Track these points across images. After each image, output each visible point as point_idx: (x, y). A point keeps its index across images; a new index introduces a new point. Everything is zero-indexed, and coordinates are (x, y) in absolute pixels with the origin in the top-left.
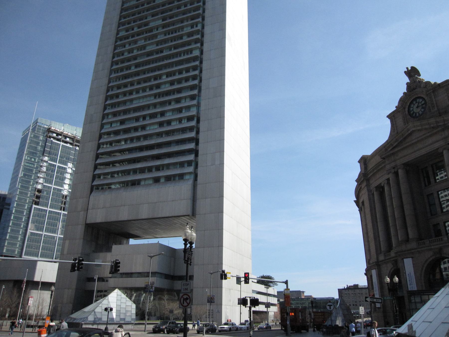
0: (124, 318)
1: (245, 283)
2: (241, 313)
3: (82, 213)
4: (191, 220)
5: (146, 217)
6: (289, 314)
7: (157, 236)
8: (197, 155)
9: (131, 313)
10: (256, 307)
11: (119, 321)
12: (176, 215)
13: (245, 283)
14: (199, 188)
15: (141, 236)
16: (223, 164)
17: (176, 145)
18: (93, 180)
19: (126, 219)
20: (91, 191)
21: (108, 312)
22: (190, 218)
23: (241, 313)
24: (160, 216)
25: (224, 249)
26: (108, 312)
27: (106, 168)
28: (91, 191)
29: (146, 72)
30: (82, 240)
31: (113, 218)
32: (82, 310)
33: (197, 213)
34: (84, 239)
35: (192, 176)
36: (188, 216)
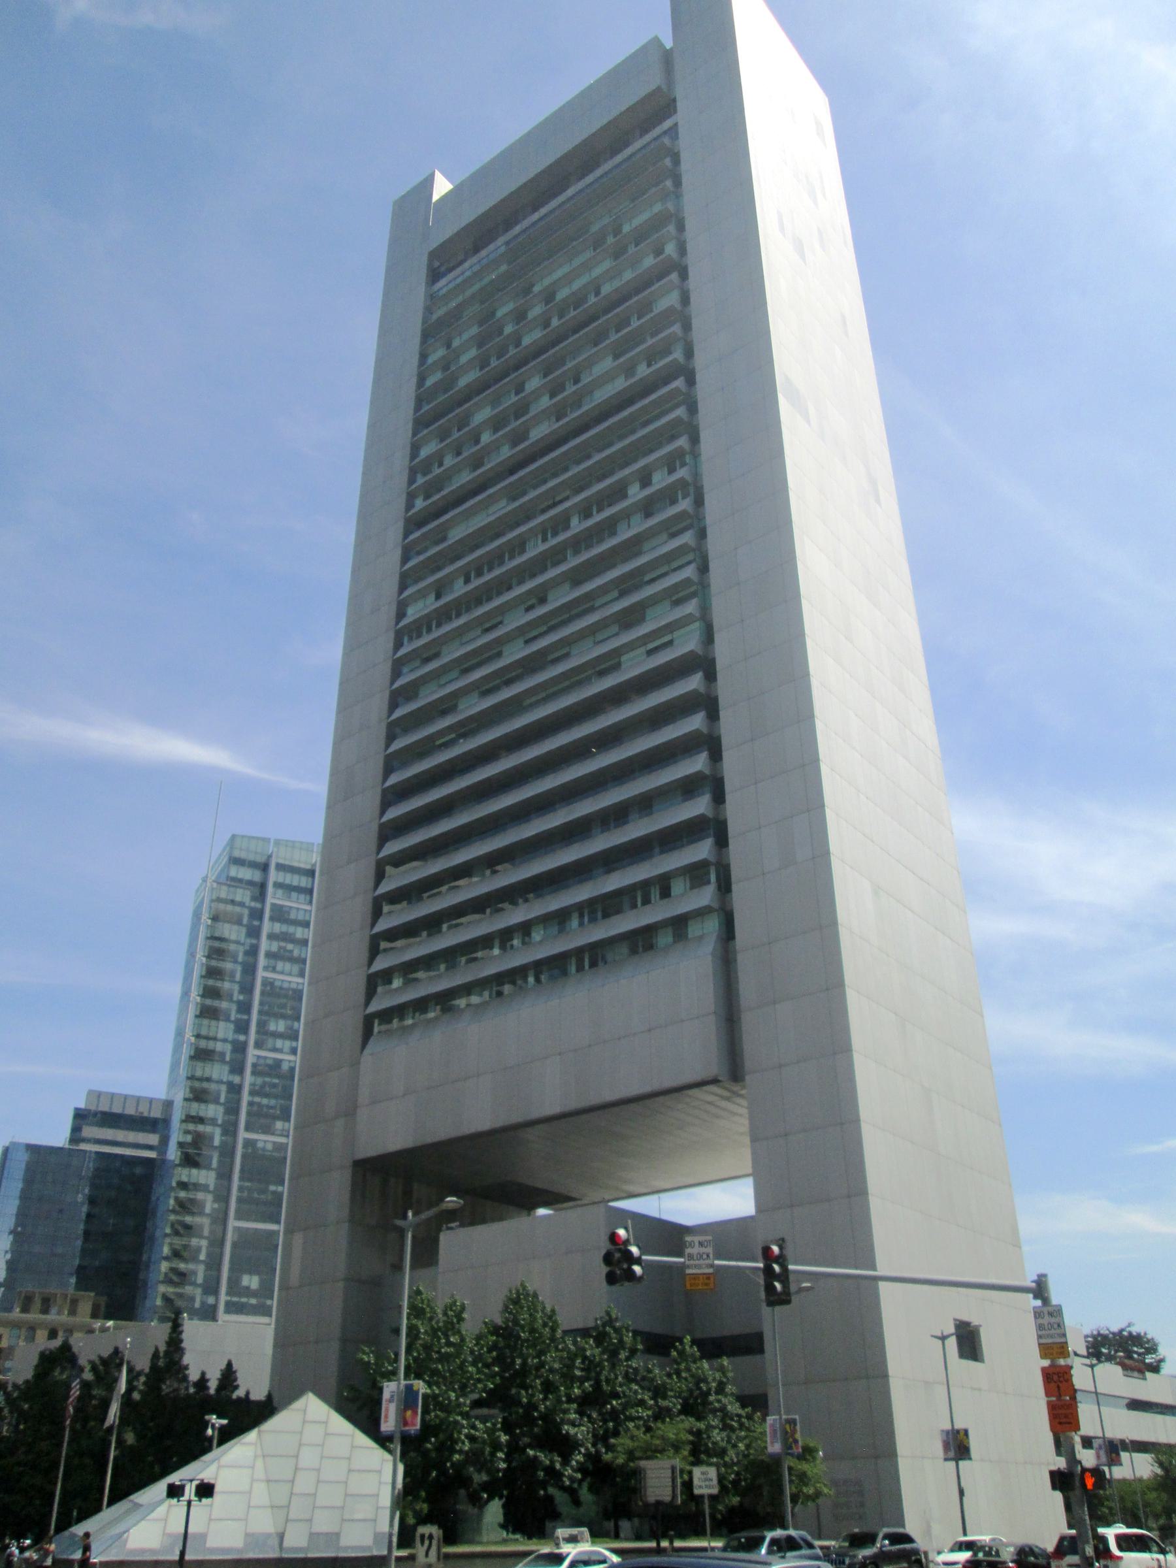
0: (336, 1530)
1: (76, 1109)
2: (961, 1493)
3: (340, 1123)
4: (734, 1103)
5: (556, 1109)
6: (1077, 1483)
7: (632, 1188)
8: (722, 841)
9: (378, 1508)
10: (234, 1369)
11: (369, 1548)
12: (669, 1083)
13: (76, 1109)
14: (745, 962)
15: (573, 1195)
16: (827, 853)
17: (640, 818)
18: (370, 993)
19: (483, 1123)
20: (367, 1034)
21: (189, 1503)
22: (726, 1094)
23: (961, 1493)
24: (609, 1096)
25: (877, 1206)
26: (189, 1503)
27: (408, 946)
28: (367, 1034)
29: (514, 581)
30: (346, 1226)
31: (441, 1129)
32: (132, 1497)
33: (748, 1064)
34: (352, 1220)
35: (712, 926)
36: (715, 1081)
